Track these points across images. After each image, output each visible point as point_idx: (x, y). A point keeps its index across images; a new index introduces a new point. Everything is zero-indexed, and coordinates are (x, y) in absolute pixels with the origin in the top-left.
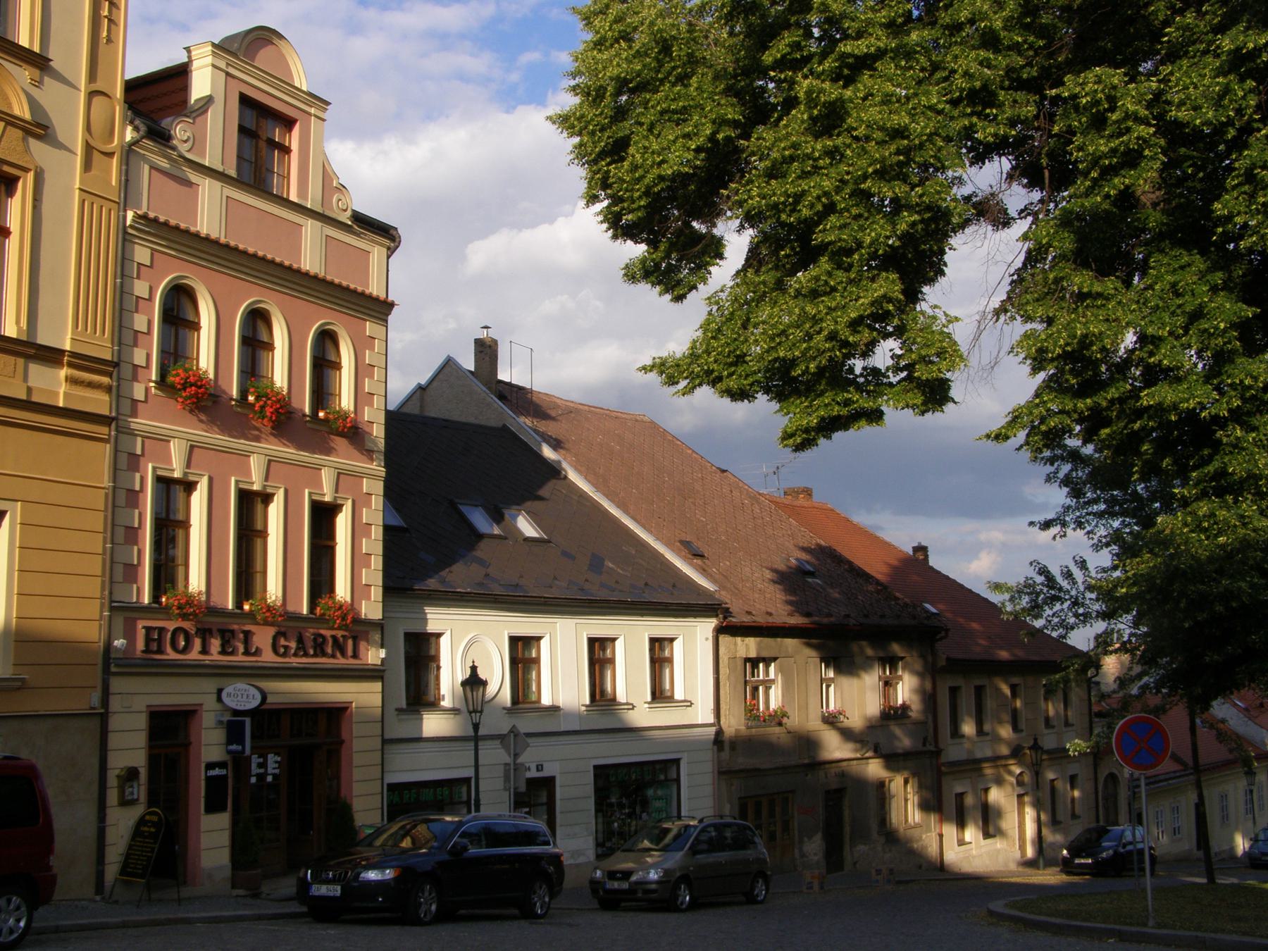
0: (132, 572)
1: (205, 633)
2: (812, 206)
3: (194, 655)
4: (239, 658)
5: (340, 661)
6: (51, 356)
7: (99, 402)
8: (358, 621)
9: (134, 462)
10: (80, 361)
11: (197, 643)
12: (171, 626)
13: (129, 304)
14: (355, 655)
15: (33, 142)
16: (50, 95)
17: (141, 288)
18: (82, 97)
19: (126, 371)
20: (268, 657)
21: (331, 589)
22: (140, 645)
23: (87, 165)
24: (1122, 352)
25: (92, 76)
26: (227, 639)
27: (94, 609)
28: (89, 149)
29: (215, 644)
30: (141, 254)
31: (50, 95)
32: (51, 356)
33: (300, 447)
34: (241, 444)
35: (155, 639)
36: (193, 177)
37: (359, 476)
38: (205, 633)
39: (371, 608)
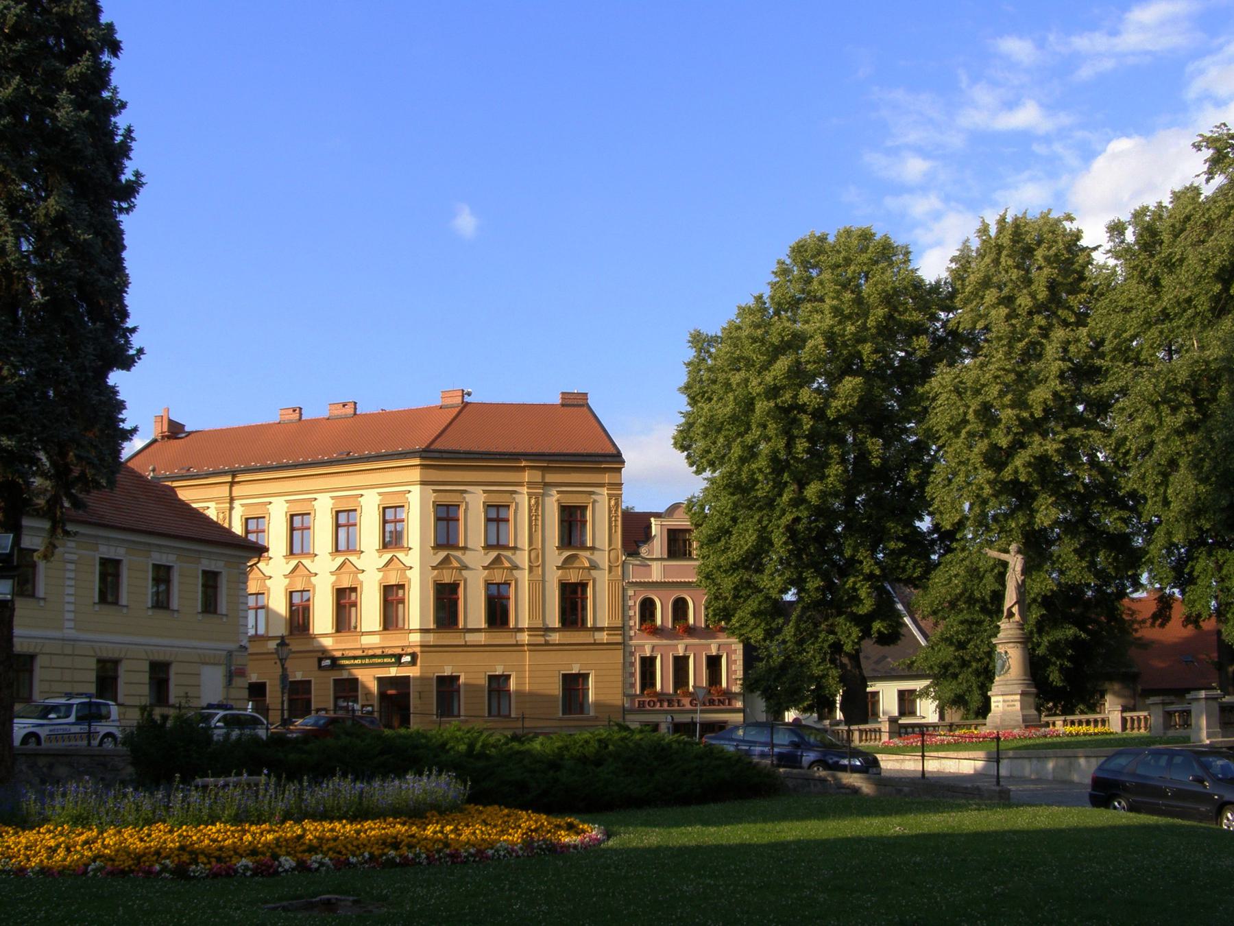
0: (633, 685)
1: (661, 701)
2: (782, 402)
3: (658, 707)
4: (676, 708)
5: (722, 707)
6: (601, 629)
7: (619, 639)
8: (731, 693)
9: (632, 654)
10: (610, 629)
11: (658, 704)
12: (648, 699)
13: (626, 608)
14: (729, 704)
15: (463, 572)
16: (597, 557)
17: (631, 603)
18: (527, 552)
19: (627, 628)
20: (688, 706)
21: (654, 685)
22: (637, 705)
23: (610, 571)
24: (778, 279)
25: (610, 545)
26: (670, 703)
27: (620, 696)
28: (610, 567)
29: (666, 704)
30: (630, 592)
31: (597, 557)
32: (601, 629)
33: (700, 638)
34: (675, 642)
35: (642, 704)
36: (649, 563)
37: (730, 644)
38: (661, 701)
39: (736, 689)
